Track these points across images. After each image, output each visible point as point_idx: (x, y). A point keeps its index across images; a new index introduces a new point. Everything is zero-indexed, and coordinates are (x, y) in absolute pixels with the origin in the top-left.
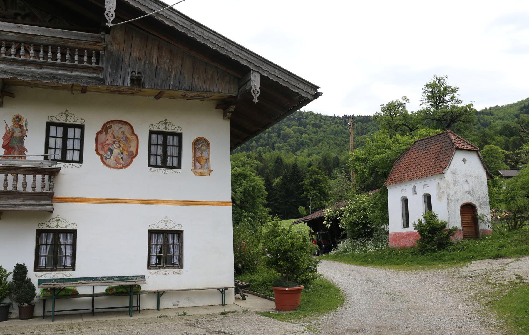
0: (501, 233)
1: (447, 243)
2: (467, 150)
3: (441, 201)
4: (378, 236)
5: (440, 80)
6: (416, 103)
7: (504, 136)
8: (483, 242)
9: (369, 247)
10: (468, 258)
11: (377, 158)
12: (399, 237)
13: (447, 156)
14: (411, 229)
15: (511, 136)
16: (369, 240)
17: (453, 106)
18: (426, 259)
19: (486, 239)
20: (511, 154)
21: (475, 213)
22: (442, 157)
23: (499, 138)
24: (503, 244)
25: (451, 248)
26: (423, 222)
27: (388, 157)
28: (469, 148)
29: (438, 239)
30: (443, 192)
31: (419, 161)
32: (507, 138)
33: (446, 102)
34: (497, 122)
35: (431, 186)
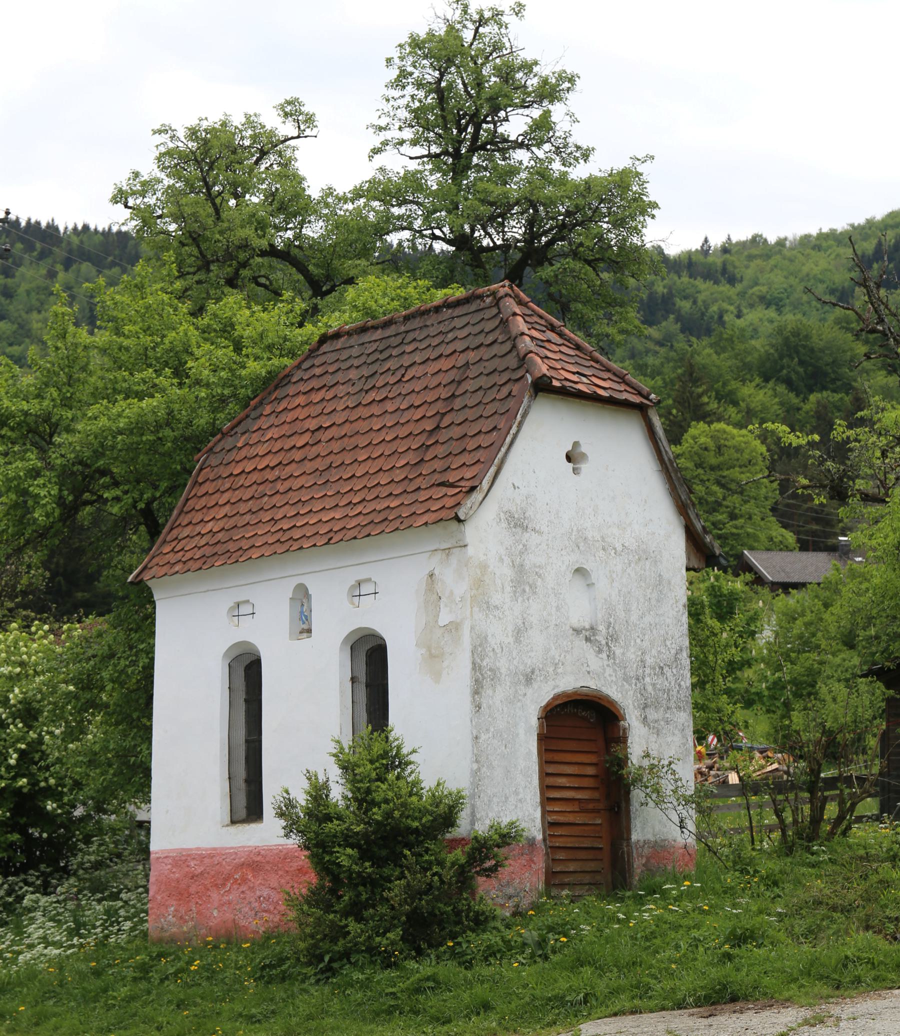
0: (742, 865)
1: (458, 913)
2: (594, 398)
3: (437, 676)
4: (98, 865)
5: (482, 21)
6: (350, 149)
7: (782, 389)
8: (651, 912)
9: (35, 932)
10: (560, 1000)
11: (103, 421)
12: (208, 872)
13: (486, 425)
14: (269, 833)
15: (811, 391)
16: (46, 889)
17: (541, 173)
18: (335, 1005)
19: (664, 894)
20: (812, 444)
21: (616, 749)
22: (456, 432)
23: (756, 394)
24: (747, 923)
25: (475, 942)
26: (338, 793)
27: (170, 420)
28: (606, 387)
29: (413, 894)
30: (454, 628)
31: (336, 446)
32: (795, 400)
33: (504, 145)
34: (753, 316)
35: (390, 589)
